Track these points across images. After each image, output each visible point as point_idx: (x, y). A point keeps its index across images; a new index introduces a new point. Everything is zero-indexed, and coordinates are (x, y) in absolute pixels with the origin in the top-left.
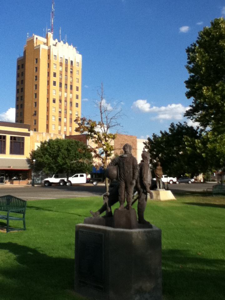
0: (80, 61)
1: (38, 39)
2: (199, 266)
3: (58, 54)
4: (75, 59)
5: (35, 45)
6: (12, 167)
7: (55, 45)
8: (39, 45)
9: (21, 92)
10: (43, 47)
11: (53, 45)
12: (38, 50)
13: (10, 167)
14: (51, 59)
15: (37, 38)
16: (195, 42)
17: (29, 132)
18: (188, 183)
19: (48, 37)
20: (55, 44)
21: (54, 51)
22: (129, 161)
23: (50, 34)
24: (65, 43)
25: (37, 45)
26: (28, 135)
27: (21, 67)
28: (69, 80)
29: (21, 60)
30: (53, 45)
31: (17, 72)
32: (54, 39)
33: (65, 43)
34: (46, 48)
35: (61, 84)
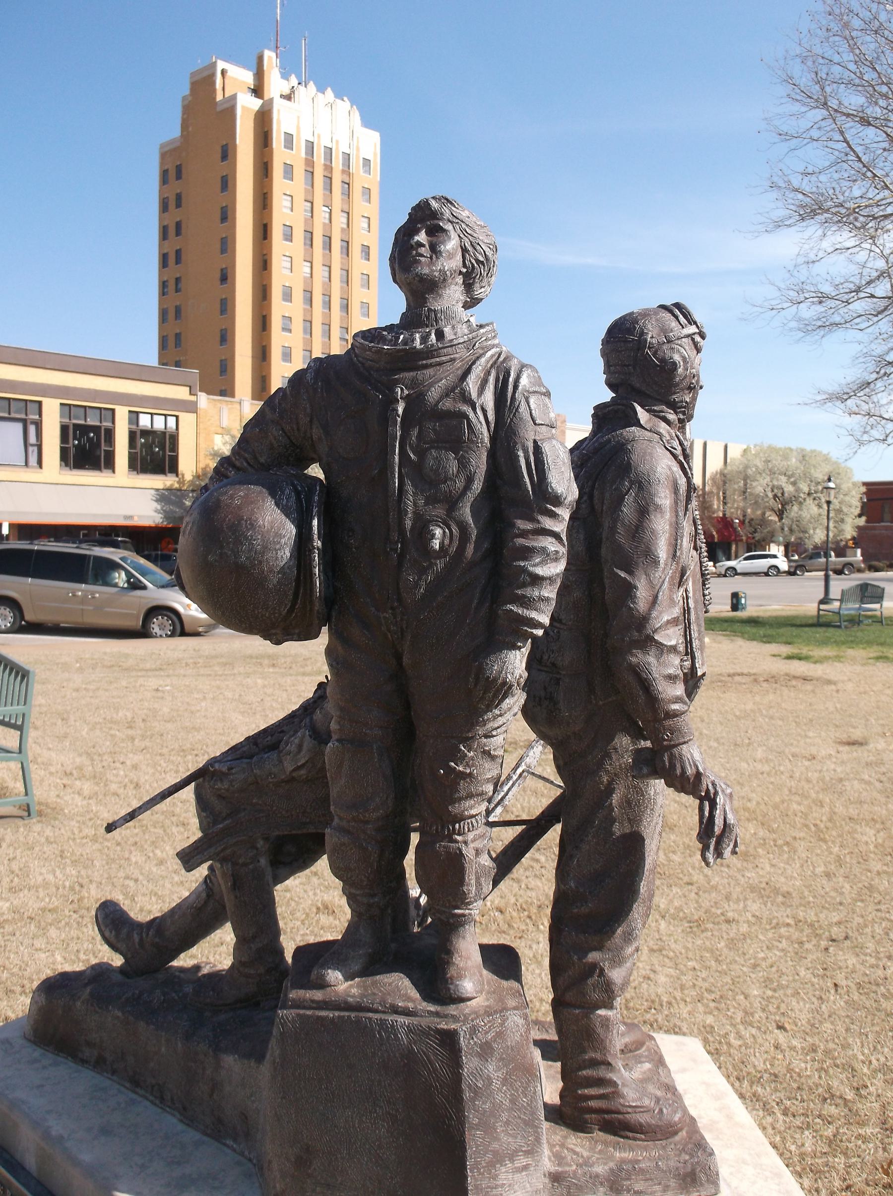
0: (375, 154)
1: (229, 74)
2: (686, 543)
3: (298, 128)
4: (358, 149)
5: (219, 97)
6: (136, 518)
7: (288, 97)
8: (234, 97)
9: (177, 263)
10: (247, 104)
11: (282, 96)
12: (229, 111)
13: (131, 517)
14: (274, 146)
15: (223, 72)
16: (706, 1185)
17: (193, 398)
18: (731, 794)
19: (265, 68)
20: (287, 91)
21: (284, 120)
22: (447, 404)
23: (270, 57)
24: (321, 89)
25: (226, 96)
26: (191, 407)
27: (172, 174)
28: (340, 220)
29: (175, 150)
30: (282, 96)
31: (161, 192)
32: (285, 76)
33: (321, 89)
34: (256, 104)
35: (309, 235)
